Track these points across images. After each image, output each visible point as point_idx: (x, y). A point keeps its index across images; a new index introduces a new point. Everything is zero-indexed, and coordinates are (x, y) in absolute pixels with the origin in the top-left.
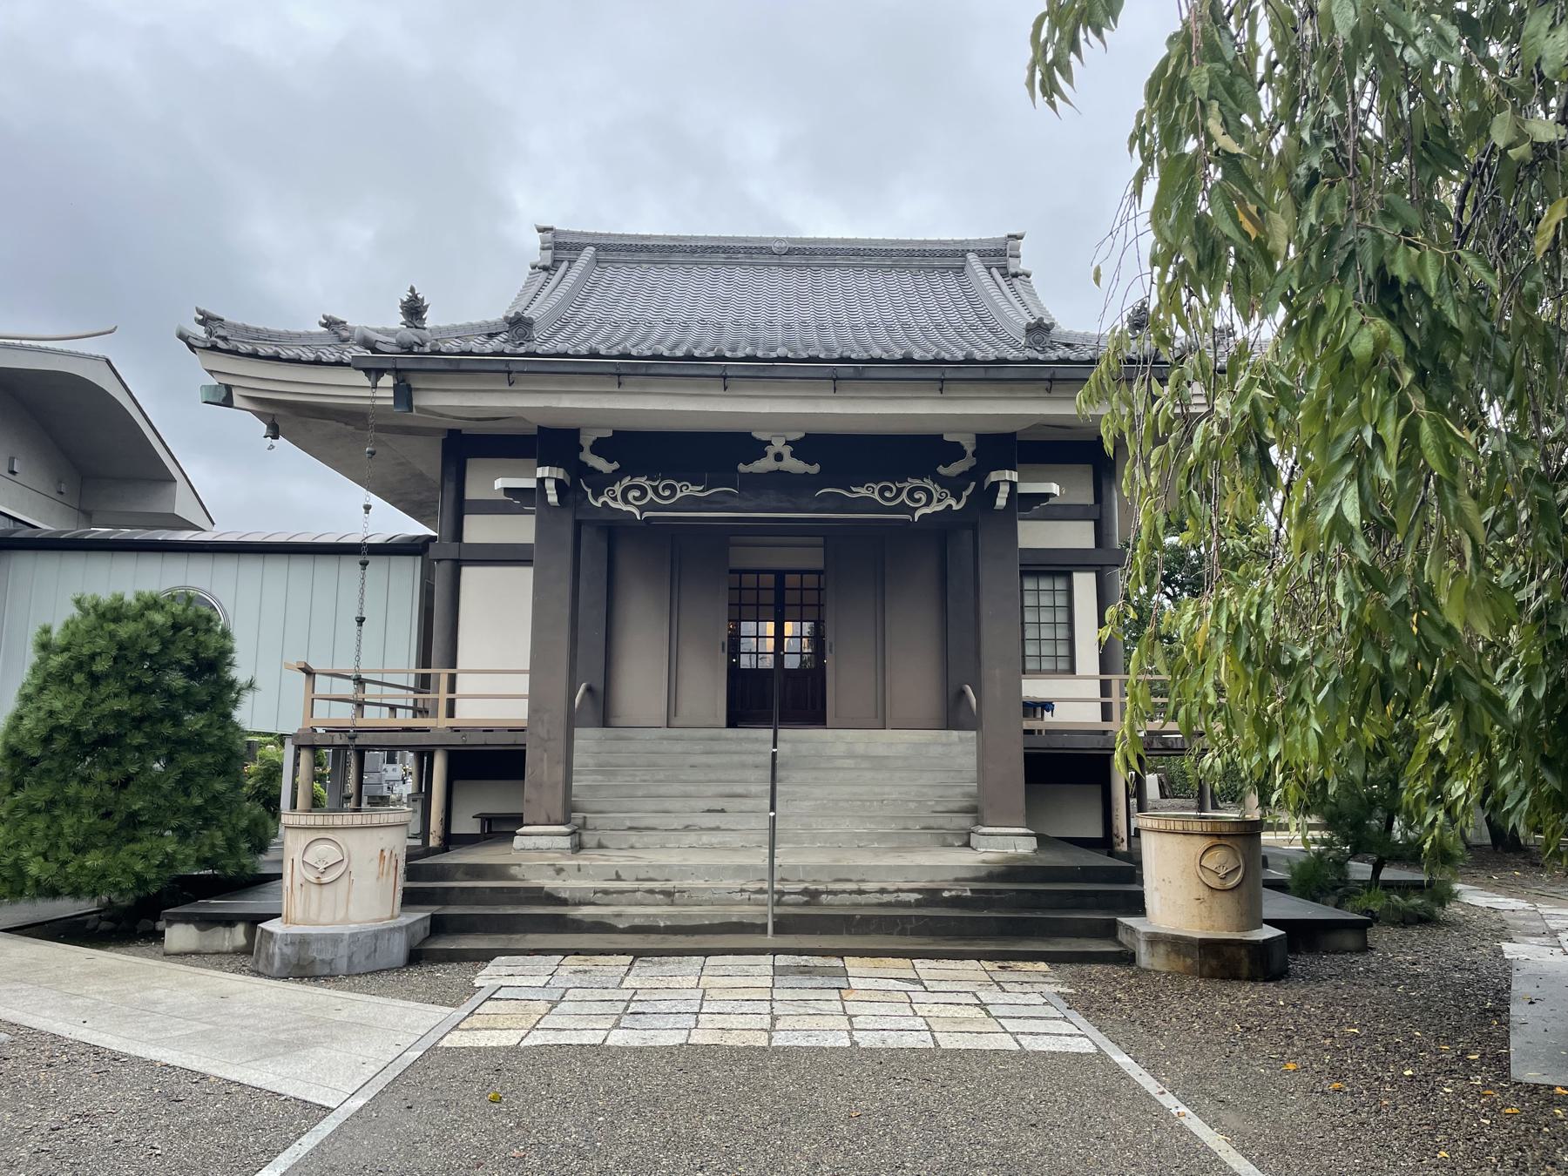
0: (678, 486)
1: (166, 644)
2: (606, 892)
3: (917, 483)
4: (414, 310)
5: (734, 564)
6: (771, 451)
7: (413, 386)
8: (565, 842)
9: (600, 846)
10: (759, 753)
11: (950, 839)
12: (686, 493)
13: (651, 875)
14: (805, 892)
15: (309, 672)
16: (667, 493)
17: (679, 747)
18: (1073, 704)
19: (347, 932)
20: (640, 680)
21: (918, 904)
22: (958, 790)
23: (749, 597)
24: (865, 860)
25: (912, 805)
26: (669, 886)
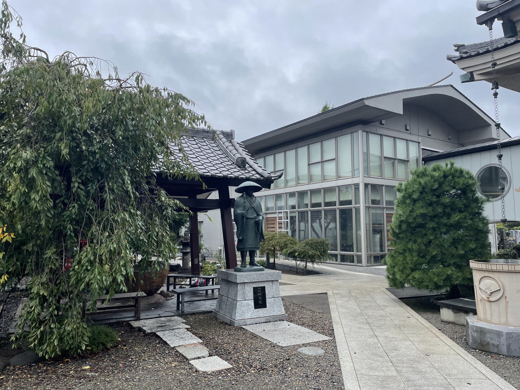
1: (441, 185)
7: (515, 19)
19: (505, 331)
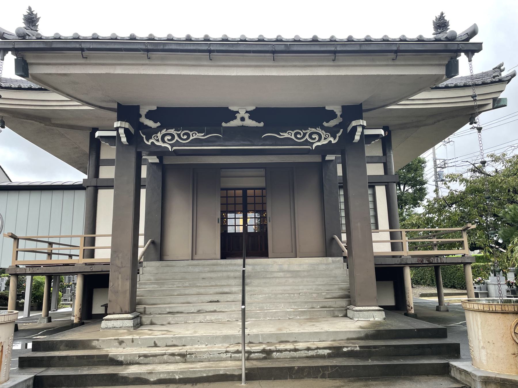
0: (191, 133)
2: (146, 356)
3: (313, 130)
4: (31, 20)
5: (224, 185)
6: (239, 116)
7: (29, 61)
8: (130, 323)
9: (152, 324)
10: (236, 271)
11: (336, 313)
12: (195, 137)
13: (175, 343)
14: (263, 351)
15: (13, 236)
16: (185, 137)
17: (197, 270)
18: (381, 244)
20: (178, 238)
21: (329, 356)
22: (336, 287)
23: (231, 200)
24: (295, 328)
25: (314, 295)
26: (183, 350)
